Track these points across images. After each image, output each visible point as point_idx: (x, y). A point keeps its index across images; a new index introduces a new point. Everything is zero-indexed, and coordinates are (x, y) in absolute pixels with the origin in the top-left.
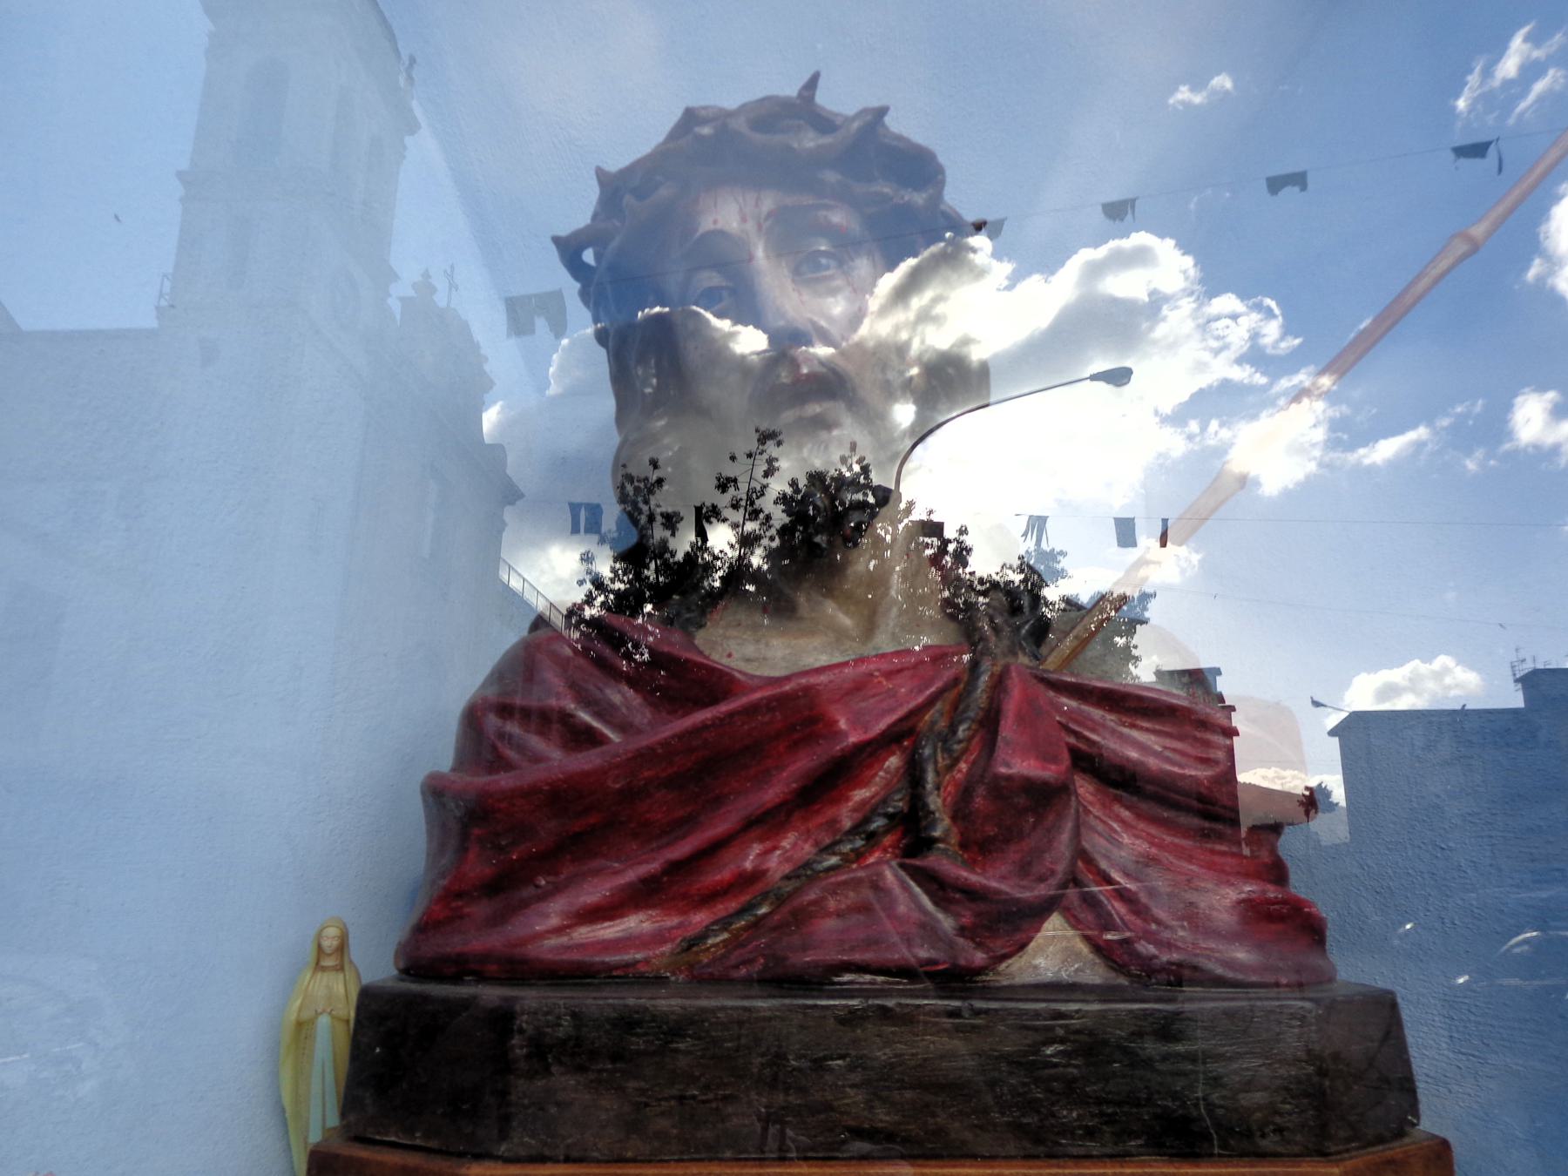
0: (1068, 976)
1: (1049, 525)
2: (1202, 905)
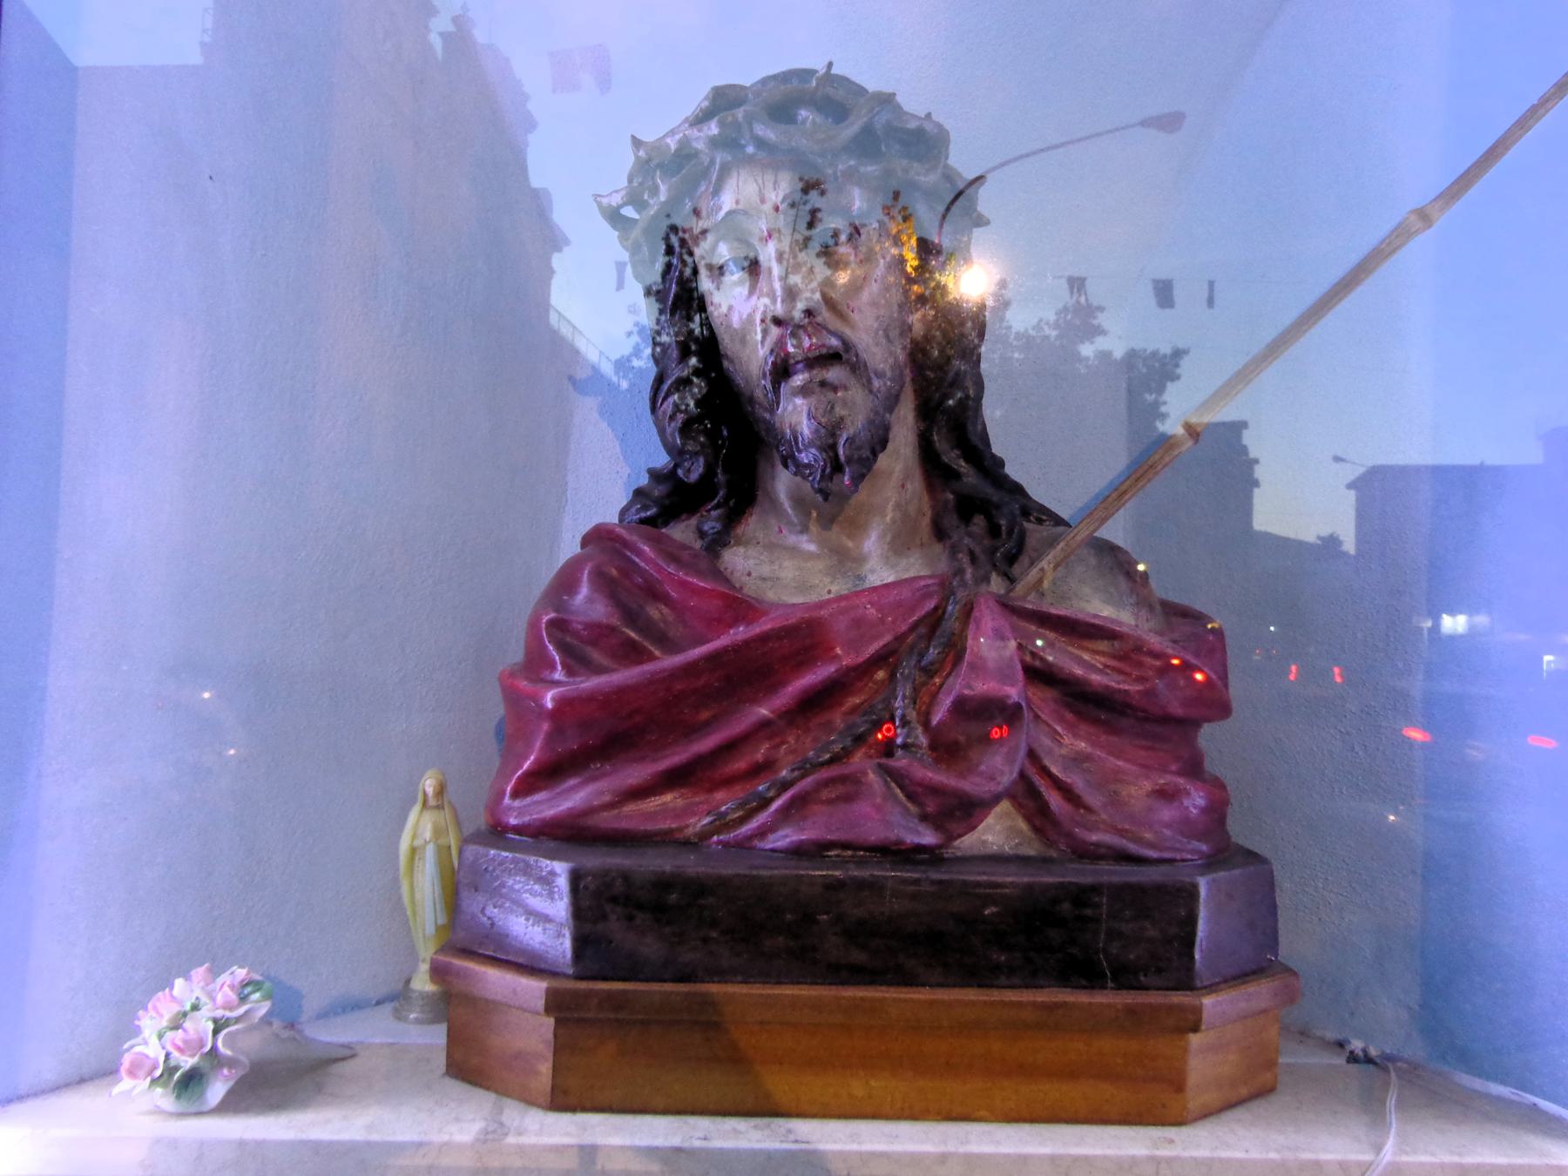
0: (1010, 848)
1: (1088, 283)
2: (1124, 793)
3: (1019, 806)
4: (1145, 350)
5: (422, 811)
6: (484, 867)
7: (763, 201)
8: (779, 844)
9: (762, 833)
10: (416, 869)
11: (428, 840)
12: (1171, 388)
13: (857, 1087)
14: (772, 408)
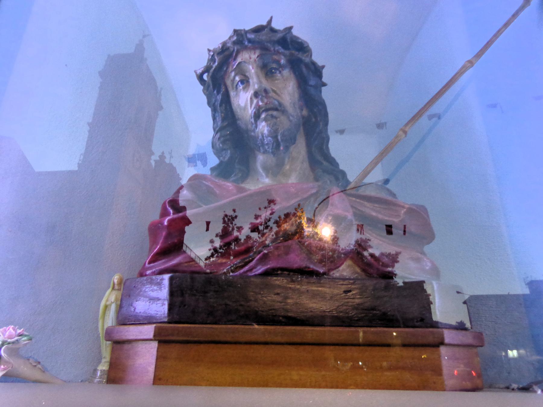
3: (355, 262)
4: (386, 253)
5: (112, 291)
6: (134, 286)
7: (250, 58)
8: (257, 273)
9: (251, 270)
10: (106, 314)
11: (113, 301)
12: (397, 265)
13: (295, 375)
14: (254, 131)
